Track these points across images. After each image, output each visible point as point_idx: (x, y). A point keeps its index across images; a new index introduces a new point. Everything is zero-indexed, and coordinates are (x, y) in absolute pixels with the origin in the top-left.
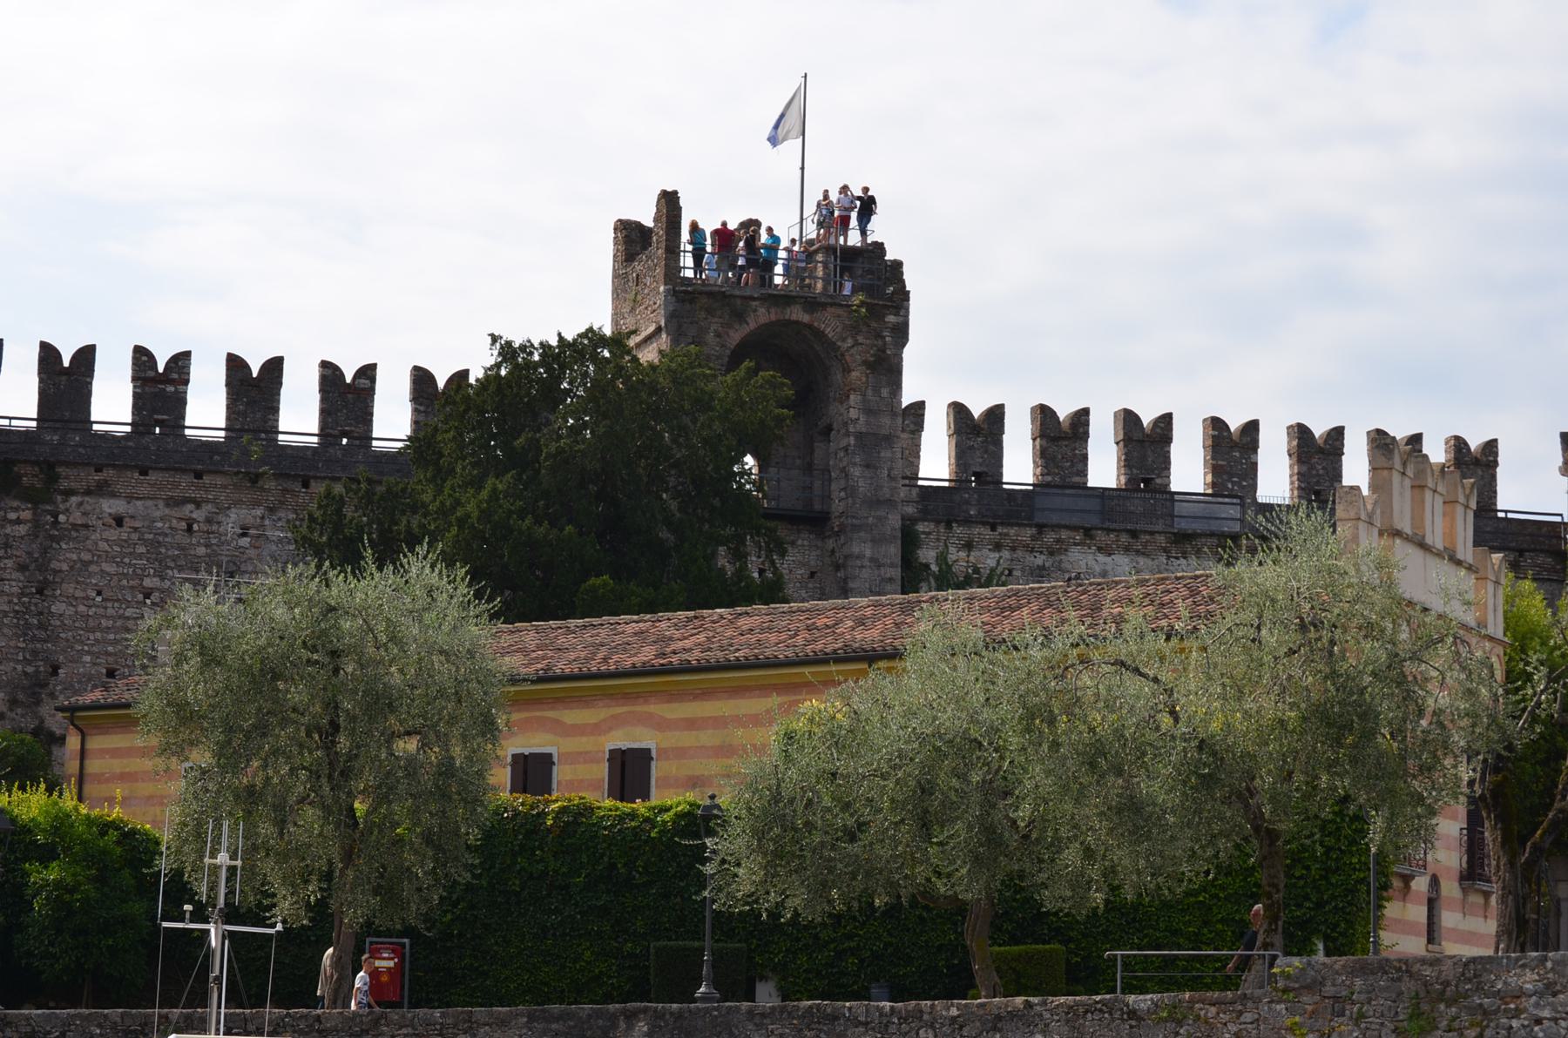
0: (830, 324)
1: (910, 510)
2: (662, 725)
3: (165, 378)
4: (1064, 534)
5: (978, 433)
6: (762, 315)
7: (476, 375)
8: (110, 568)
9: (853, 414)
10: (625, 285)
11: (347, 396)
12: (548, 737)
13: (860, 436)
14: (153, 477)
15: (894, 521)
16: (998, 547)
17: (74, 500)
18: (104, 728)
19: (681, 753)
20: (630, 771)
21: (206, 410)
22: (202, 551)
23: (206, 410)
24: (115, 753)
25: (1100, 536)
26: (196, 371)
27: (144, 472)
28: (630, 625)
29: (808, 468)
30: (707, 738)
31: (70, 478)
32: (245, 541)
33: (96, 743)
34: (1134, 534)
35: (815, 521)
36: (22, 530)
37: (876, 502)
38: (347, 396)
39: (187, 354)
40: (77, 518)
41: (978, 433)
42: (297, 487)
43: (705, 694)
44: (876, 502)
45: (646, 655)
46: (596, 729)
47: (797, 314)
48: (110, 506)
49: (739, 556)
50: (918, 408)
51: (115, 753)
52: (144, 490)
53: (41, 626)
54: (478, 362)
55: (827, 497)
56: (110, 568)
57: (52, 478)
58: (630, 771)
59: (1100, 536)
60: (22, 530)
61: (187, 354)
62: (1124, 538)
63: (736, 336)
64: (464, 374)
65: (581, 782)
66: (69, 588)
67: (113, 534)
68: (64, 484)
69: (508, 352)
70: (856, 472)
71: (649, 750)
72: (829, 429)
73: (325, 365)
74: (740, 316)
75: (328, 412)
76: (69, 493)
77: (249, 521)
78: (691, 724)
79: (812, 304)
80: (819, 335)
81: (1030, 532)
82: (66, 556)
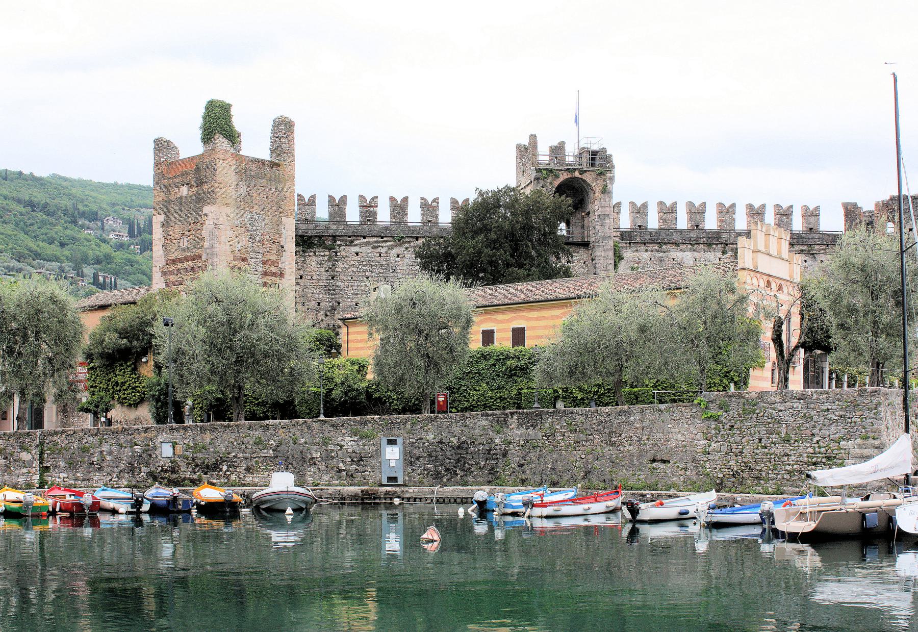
0: (588, 177)
1: (617, 239)
2: (528, 319)
3: (728, 212)
4: (669, 245)
5: (640, 210)
6: (564, 176)
7: (471, 201)
8: (355, 270)
9: (596, 208)
10: (522, 168)
11: (430, 208)
12: (493, 324)
13: (599, 215)
14: (367, 239)
15: (611, 244)
16: (647, 251)
17: (342, 248)
18: (354, 324)
19: (534, 328)
20: (518, 335)
21: (384, 216)
22: (384, 263)
23: (384, 216)
24: (358, 333)
25: (681, 245)
26: (737, 209)
27: (364, 237)
28: (519, 286)
29: (583, 227)
30: (542, 323)
31: (340, 241)
32: (398, 259)
33: (351, 330)
34: (692, 245)
35: (585, 245)
36: (326, 258)
37: (604, 238)
38: (430, 208)
39: (345, 197)
40: (343, 253)
41: (640, 210)
42: (415, 240)
43: (541, 309)
44: (604, 238)
45: (522, 297)
46: (508, 321)
47: (577, 174)
48: (354, 249)
49: (558, 258)
50: (619, 205)
51: (358, 333)
52: (364, 244)
53: (334, 290)
54: (473, 197)
55: (589, 236)
56: (355, 270)
57: (335, 241)
58: (518, 335)
59: (681, 245)
60: (326, 258)
61: (345, 197)
62: (689, 246)
63: (557, 183)
64: (467, 200)
65: (503, 342)
66: (342, 277)
67: (356, 258)
68: (338, 243)
69: (481, 194)
70: (597, 227)
71: (493, 342)
72: (589, 213)
73: (330, 196)
74: (557, 177)
75: (362, 214)
76: (340, 246)
77: (399, 252)
78: (537, 319)
79: (582, 172)
80: (584, 181)
81: (657, 245)
82: (340, 267)
